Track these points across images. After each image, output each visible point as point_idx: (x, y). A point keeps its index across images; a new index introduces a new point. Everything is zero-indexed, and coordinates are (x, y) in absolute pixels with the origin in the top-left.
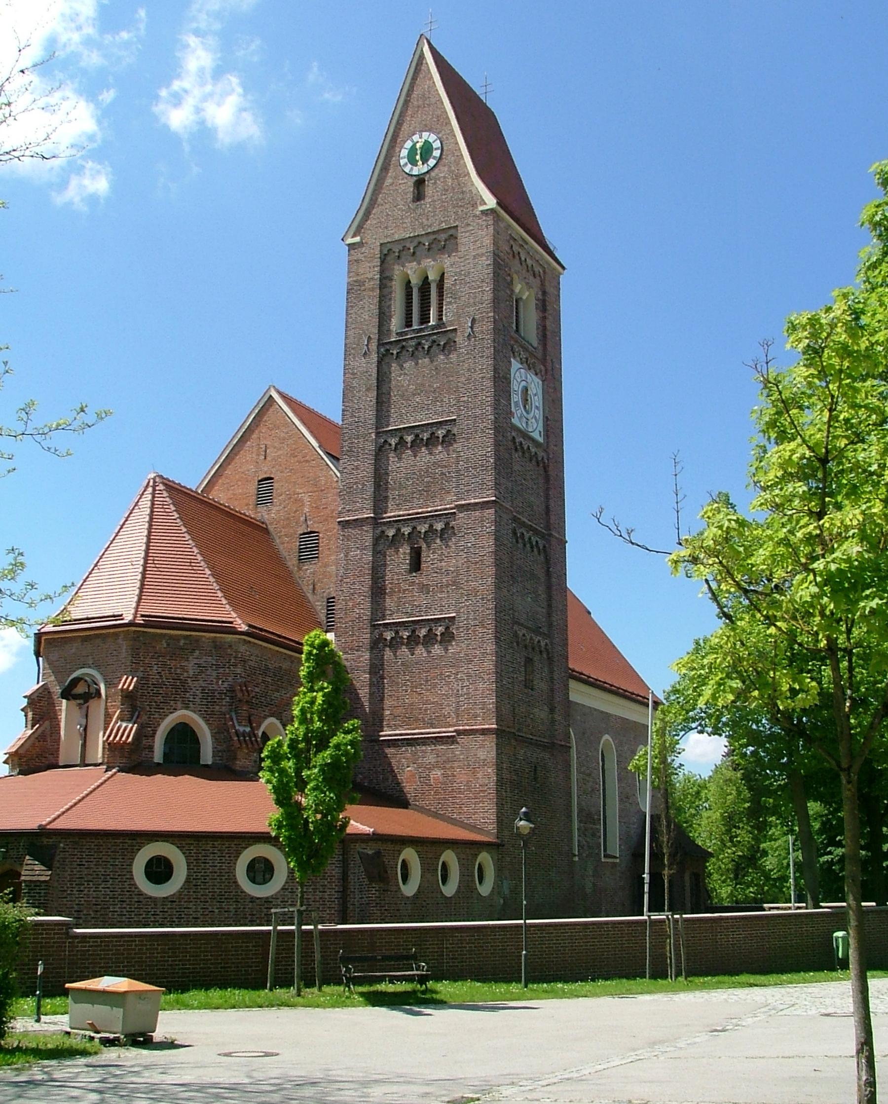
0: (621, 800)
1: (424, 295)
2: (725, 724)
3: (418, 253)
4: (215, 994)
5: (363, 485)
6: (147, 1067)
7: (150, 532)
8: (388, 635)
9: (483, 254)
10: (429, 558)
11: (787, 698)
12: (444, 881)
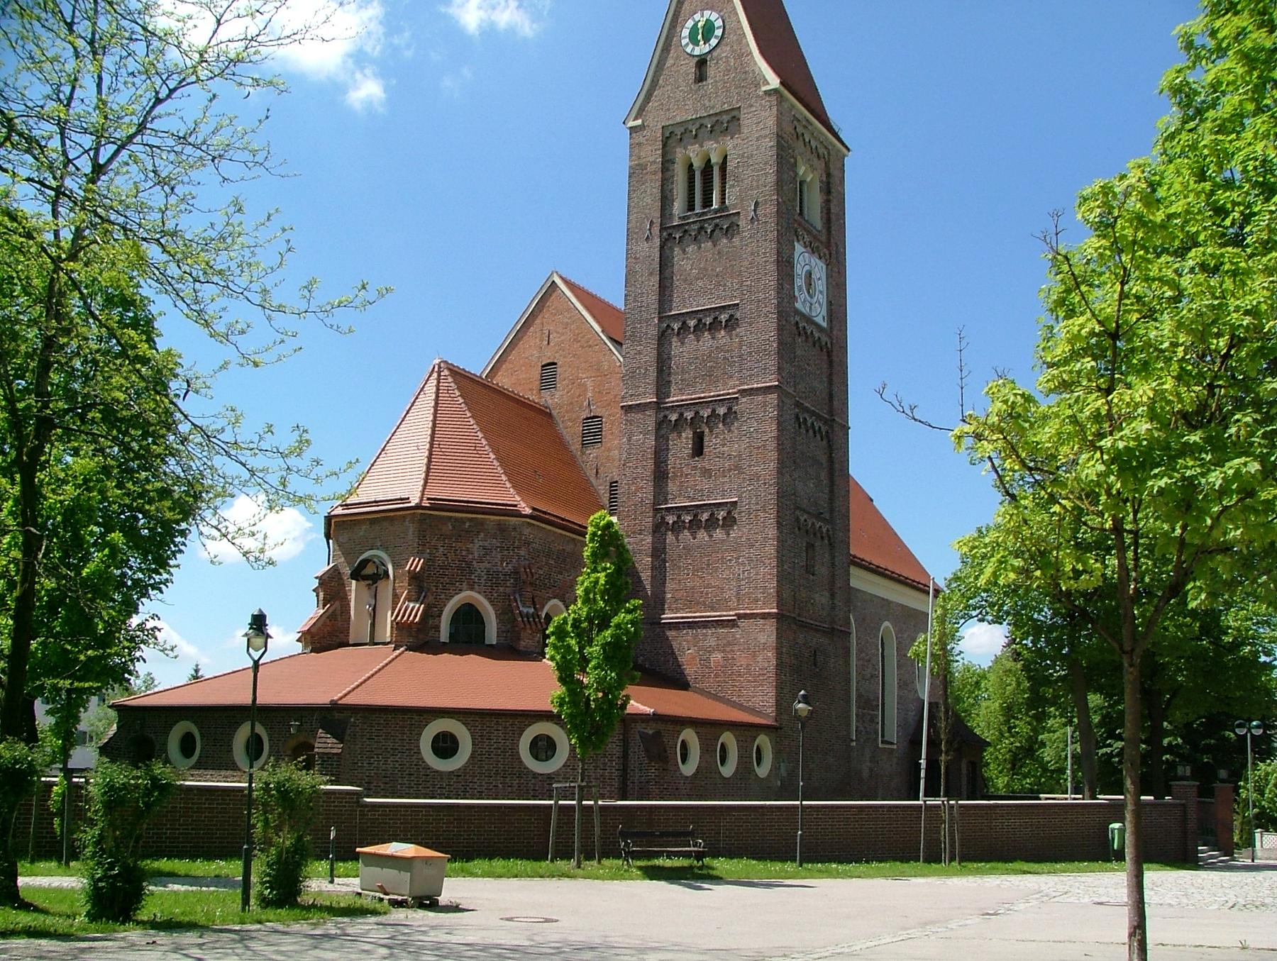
1: (707, 178)
2: (1008, 613)
3: (700, 136)
4: (498, 864)
6: (433, 928)
8: (671, 519)
9: (766, 136)
10: (710, 442)
11: (1070, 578)
12: (723, 761)
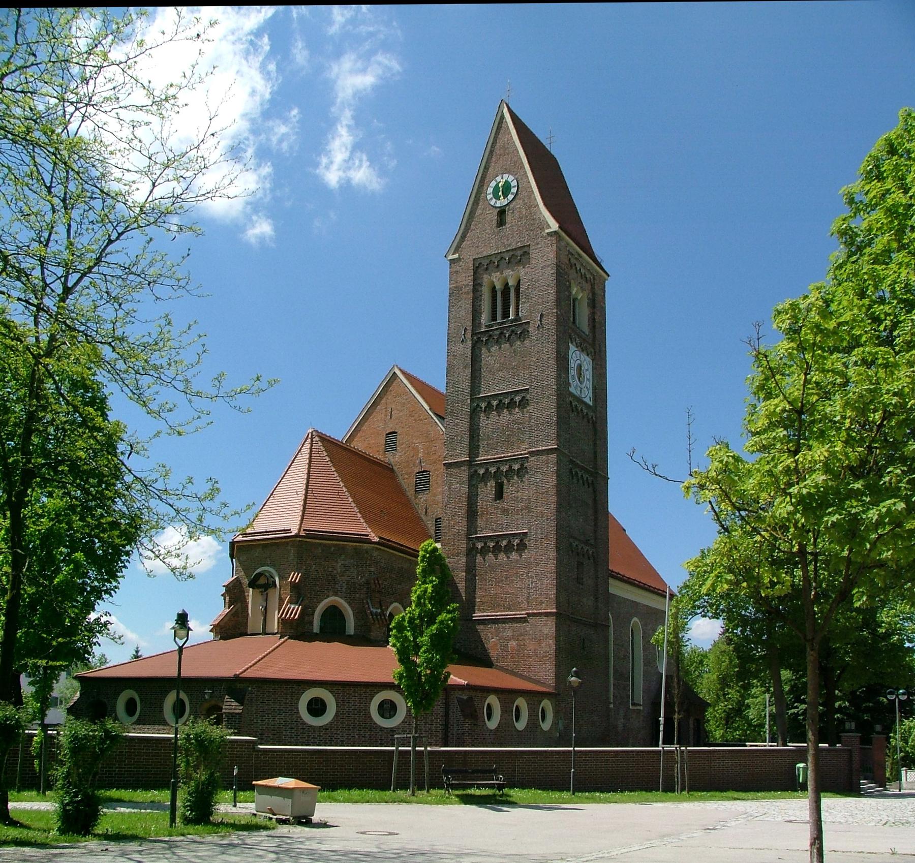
0: (645, 665)
1: (505, 296)
2: (723, 611)
4: (355, 793)
5: (462, 437)
6: (308, 839)
7: (309, 471)
8: (479, 545)
9: (548, 266)
10: (508, 489)
11: (767, 588)
12: (517, 719)
